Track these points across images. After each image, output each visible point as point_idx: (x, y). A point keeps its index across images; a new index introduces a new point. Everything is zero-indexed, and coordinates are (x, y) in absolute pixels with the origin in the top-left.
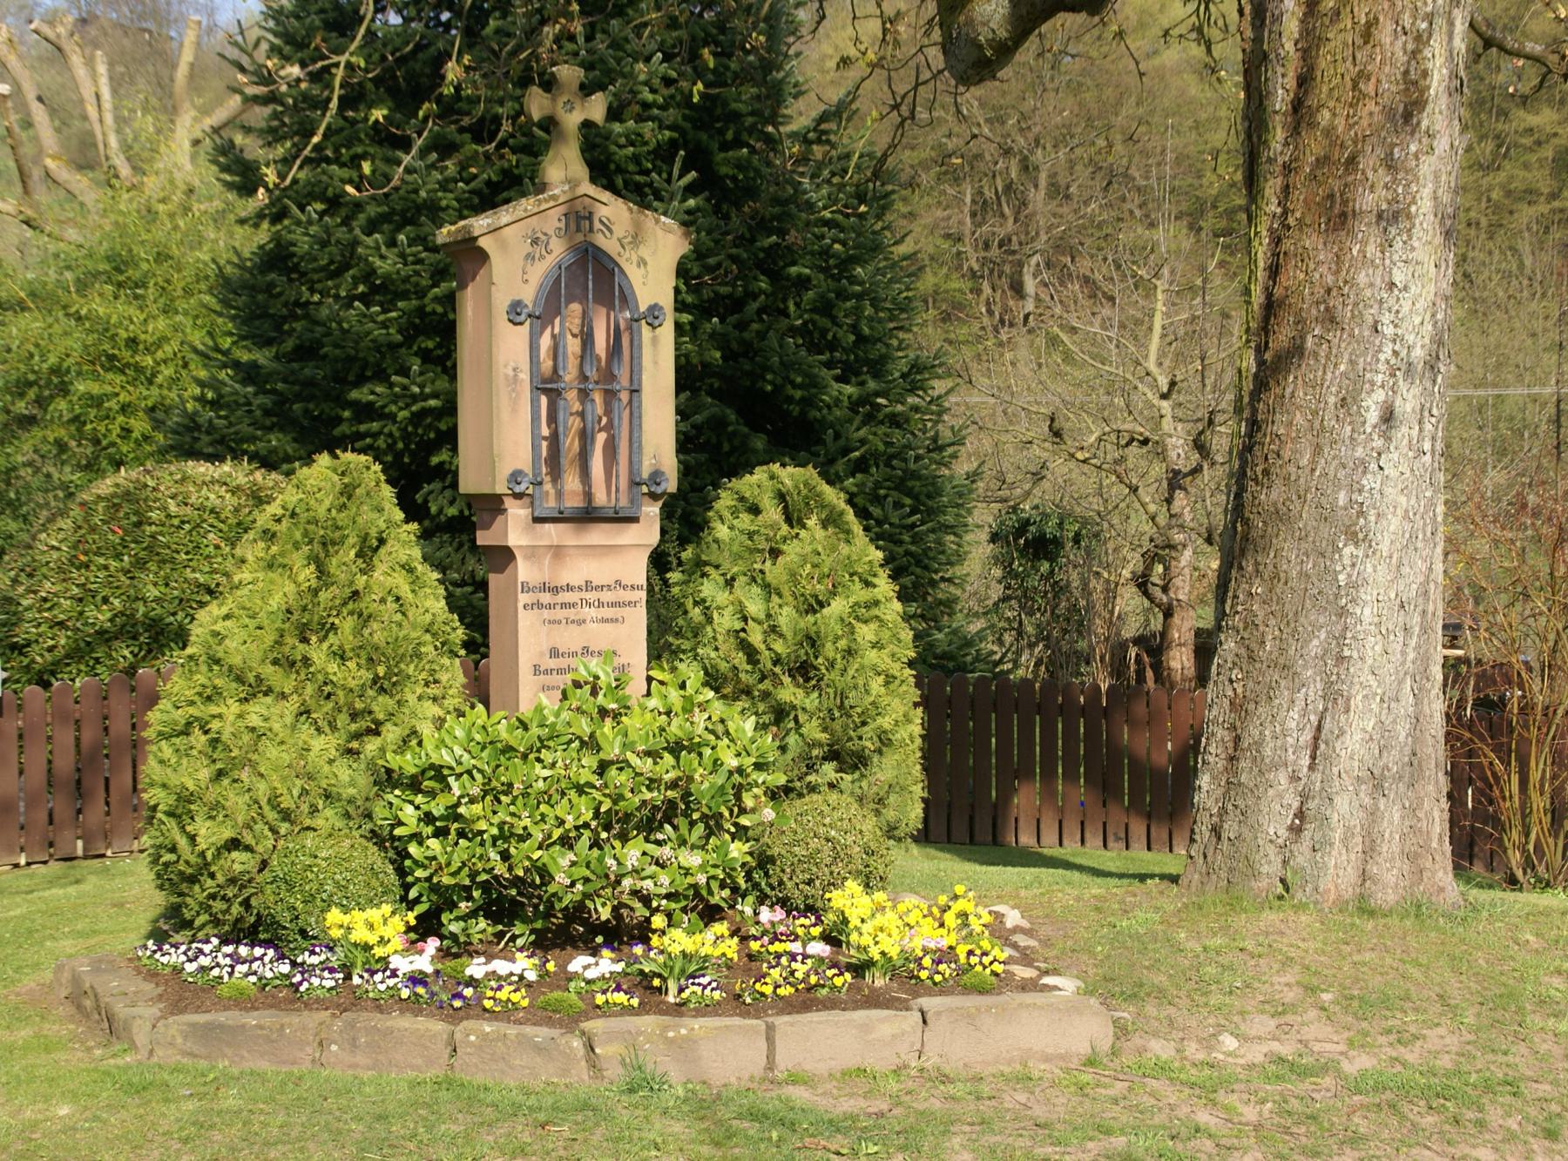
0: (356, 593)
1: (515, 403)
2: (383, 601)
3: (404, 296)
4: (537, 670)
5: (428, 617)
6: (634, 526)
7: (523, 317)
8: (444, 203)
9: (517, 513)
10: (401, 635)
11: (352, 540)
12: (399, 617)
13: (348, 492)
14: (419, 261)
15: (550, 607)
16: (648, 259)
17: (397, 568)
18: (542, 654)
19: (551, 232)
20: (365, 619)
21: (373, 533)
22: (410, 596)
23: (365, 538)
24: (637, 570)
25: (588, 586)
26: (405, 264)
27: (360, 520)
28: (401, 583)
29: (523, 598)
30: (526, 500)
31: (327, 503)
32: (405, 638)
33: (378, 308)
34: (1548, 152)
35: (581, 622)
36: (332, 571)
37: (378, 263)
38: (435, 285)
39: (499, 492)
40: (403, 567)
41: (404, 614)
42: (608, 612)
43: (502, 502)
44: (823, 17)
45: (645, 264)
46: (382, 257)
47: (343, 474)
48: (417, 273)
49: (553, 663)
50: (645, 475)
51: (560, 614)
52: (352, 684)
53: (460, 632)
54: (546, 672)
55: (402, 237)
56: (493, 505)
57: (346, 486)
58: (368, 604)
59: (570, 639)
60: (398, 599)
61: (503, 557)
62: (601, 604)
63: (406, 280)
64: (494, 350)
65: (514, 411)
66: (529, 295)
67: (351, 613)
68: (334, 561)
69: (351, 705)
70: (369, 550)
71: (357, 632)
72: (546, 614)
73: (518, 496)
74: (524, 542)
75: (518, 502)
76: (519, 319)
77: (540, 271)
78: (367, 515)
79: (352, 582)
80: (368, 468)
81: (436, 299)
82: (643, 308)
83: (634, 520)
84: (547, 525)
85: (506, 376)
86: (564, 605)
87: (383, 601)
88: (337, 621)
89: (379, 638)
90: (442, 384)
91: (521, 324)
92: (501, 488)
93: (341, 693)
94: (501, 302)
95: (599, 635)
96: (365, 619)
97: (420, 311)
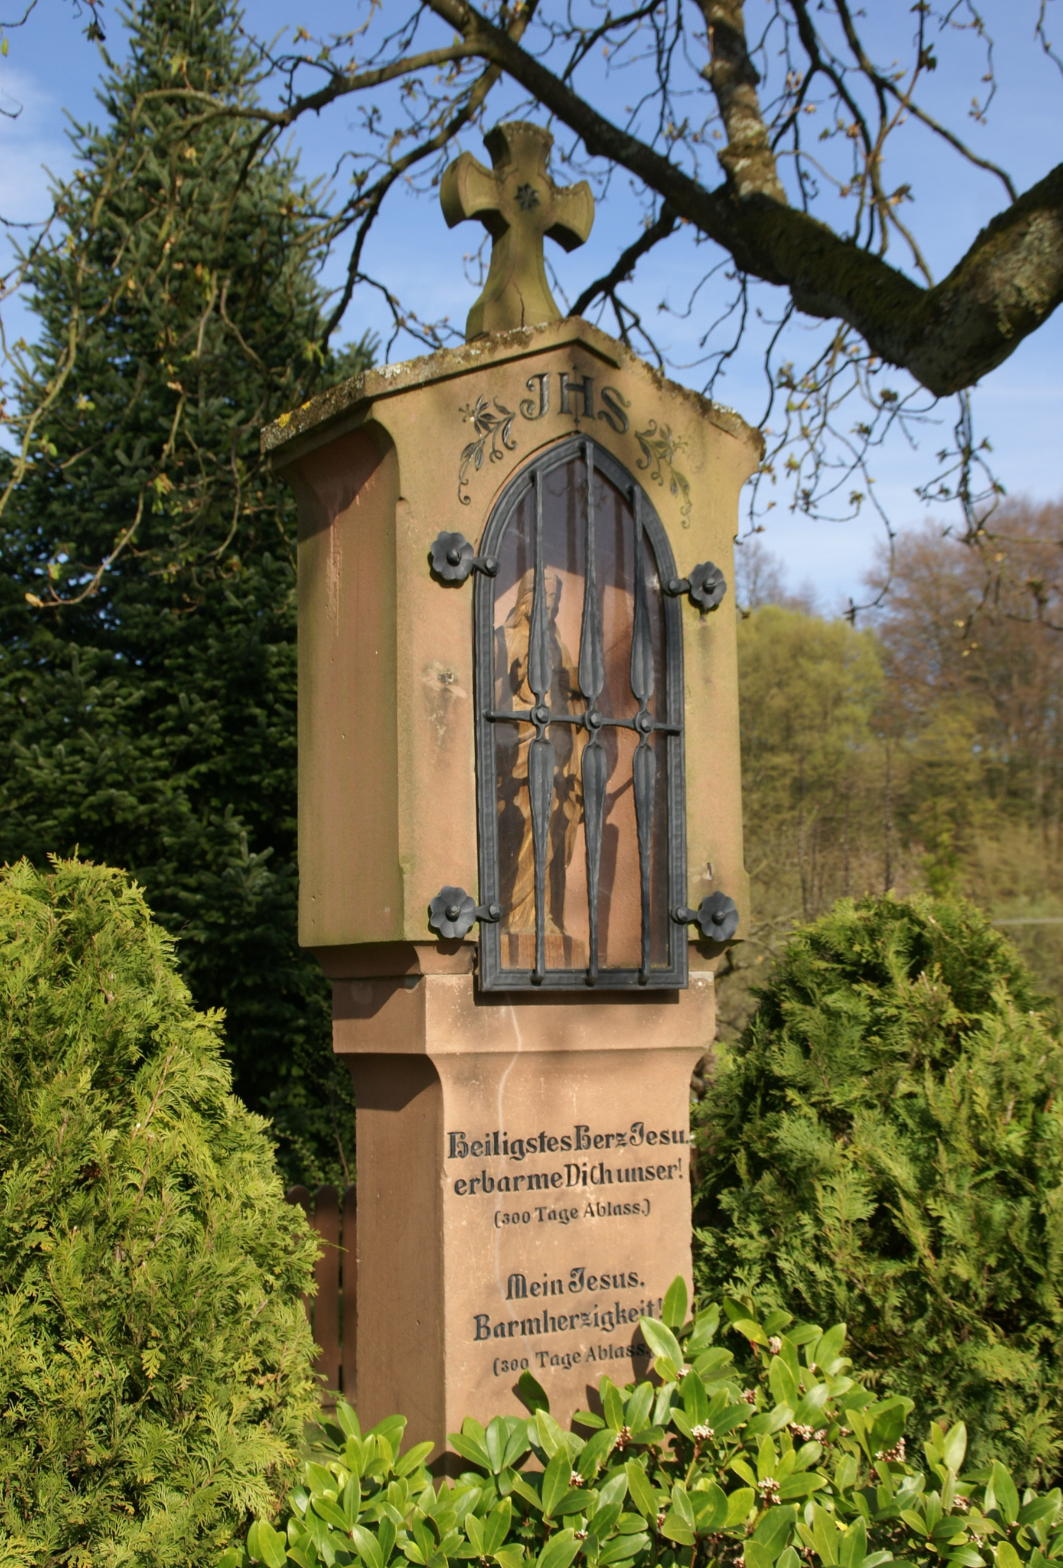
0: (91, 1170)
1: (444, 745)
2: (154, 1186)
3: (61, 805)
4: (482, 1327)
5: (254, 1219)
6: (670, 1008)
7: (462, 570)
8: (101, 717)
9: (444, 980)
10: (194, 1267)
11: (84, 1048)
12: (186, 1223)
13: (74, 941)
14: (77, 771)
15: (508, 1184)
16: (690, 478)
17: (185, 1109)
18: (491, 1289)
19: (513, 407)
20: (115, 1231)
21: (132, 1031)
22: (213, 1170)
23: (113, 1043)
24: (669, 1102)
25: (582, 1137)
26: (63, 773)
27: (98, 1002)
28: (190, 1138)
29: (454, 1169)
30: (464, 956)
31: (29, 965)
32: (206, 1271)
33: (34, 817)
34: (787, 781)
35: (568, 1216)
36: (37, 1120)
37: (35, 772)
38: (92, 793)
39: (410, 936)
40: (195, 1106)
41: (201, 1216)
42: (619, 1192)
43: (415, 959)
44: (1038, 28)
45: (686, 487)
46: (39, 767)
47: (63, 902)
48: (72, 782)
49: (514, 1310)
50: (693, 902)
51: (527, 1199)
52: (79, 1397)
53: (312, 1246)
54: (504, 1330)
55: (60, 747)
56: (388, 966)
57: (70, 929)
58: (120, 1198)
59: (547, 1253)
60: (187, 1182)
61: (411, 1075)
62: (605, 1175)
63: (63, 790)
64: (402, 637)
65: (443, 765)
66: (470, 526)
67: (79, 1219)
68: (42, 1097)
69: (75, 1451)
70: (120, 1069)
71: (93, 1269)
72: (500, 1200)
73: (447, 946)
74: (457, 1047)
75: (447, 960)
76: (452, 573)
77: (491, 481)
78: (118, 991)
79: (82, 1145)
80: (117, 893)
81: (91, 807)
82: (684, 571)
83: (666, 996)
84: (503, 1009)
85: (426, 690)
86: (537, 1181)
87: (154, 1186)
88: (47, 1246)
89: (146, 1278)
90: (291, 713)
91: (456, 583)
92: (415, 929)
93: (50, 1423)
94: (417, 537)
95: (602, 1242)
96: (115, 1231)
97: (76, 819)
